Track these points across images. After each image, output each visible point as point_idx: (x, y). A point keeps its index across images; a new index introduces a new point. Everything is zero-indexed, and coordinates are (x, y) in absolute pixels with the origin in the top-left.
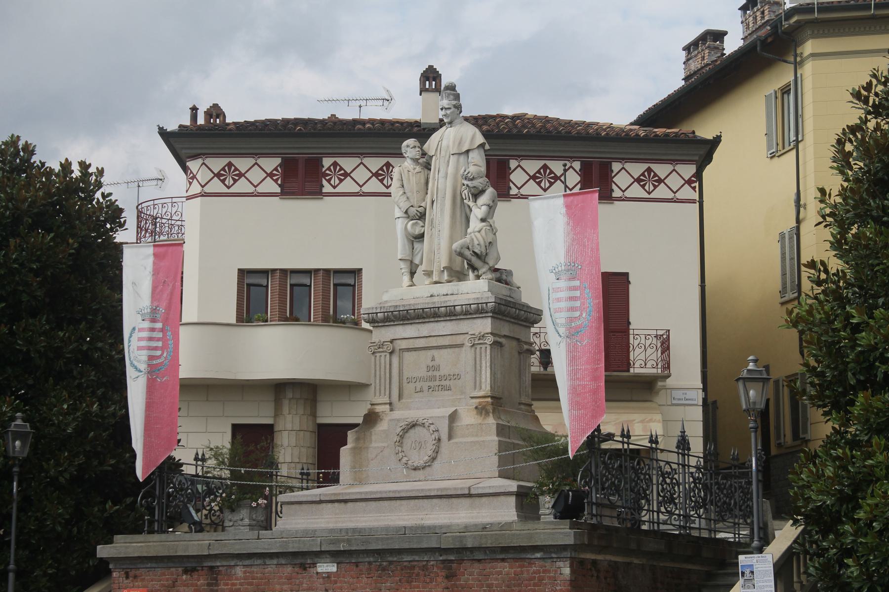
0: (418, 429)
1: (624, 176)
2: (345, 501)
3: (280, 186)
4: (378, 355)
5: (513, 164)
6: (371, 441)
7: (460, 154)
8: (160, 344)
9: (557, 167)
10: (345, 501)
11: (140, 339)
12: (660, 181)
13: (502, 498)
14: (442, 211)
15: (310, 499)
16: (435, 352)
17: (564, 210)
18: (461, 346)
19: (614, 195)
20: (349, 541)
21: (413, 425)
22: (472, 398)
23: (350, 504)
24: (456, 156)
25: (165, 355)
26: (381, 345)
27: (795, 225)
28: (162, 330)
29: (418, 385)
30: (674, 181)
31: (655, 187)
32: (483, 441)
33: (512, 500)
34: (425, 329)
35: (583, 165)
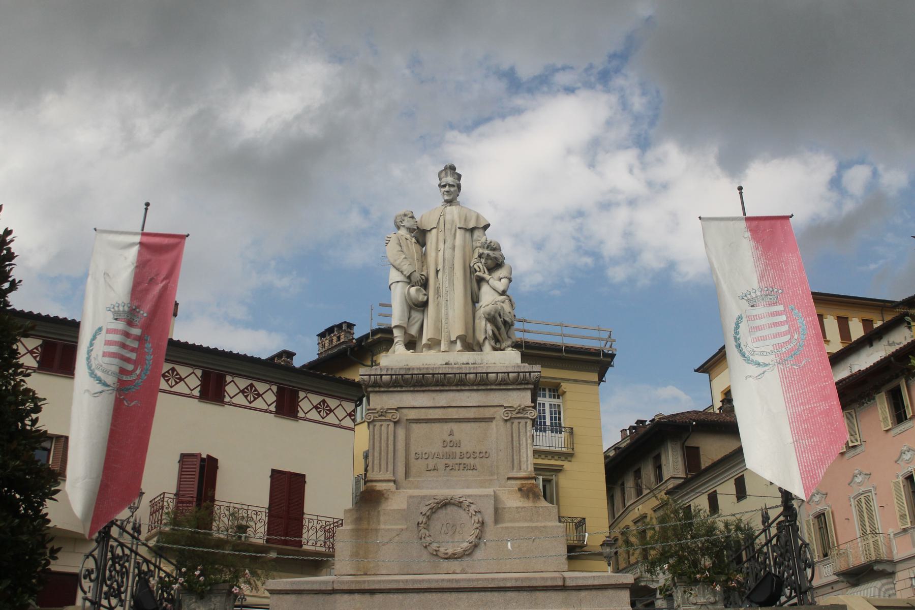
0: (450, 509)
1: (307, 403)
2: (372, 592)
3: (38, 362)
4: (378, 424)
5: (229, 378)
6: (379, 522)
7: (466, 230)
8: (133, 356)
9: (261, 387)
10: (372, 592)
11: (108, 343)
13: (610, 593)
14: (451, 282)
15: (316, 587)
16: (455, 426)
17: (748, 234)
18: (491, 420)
19: (299, 415)
21: (445, 504)
22: (509, 479)
23: (379, 597)
24: (463, 231)
25: (138, 372)
26: (383, 413)
27: (363, 472)
28: (140, 339)
29: (431, 463)
30: (340, 413)
31: (327, 414)
32: (544, 527)
33: (625, 595)
34: (443, 399)
35: (278, 388)
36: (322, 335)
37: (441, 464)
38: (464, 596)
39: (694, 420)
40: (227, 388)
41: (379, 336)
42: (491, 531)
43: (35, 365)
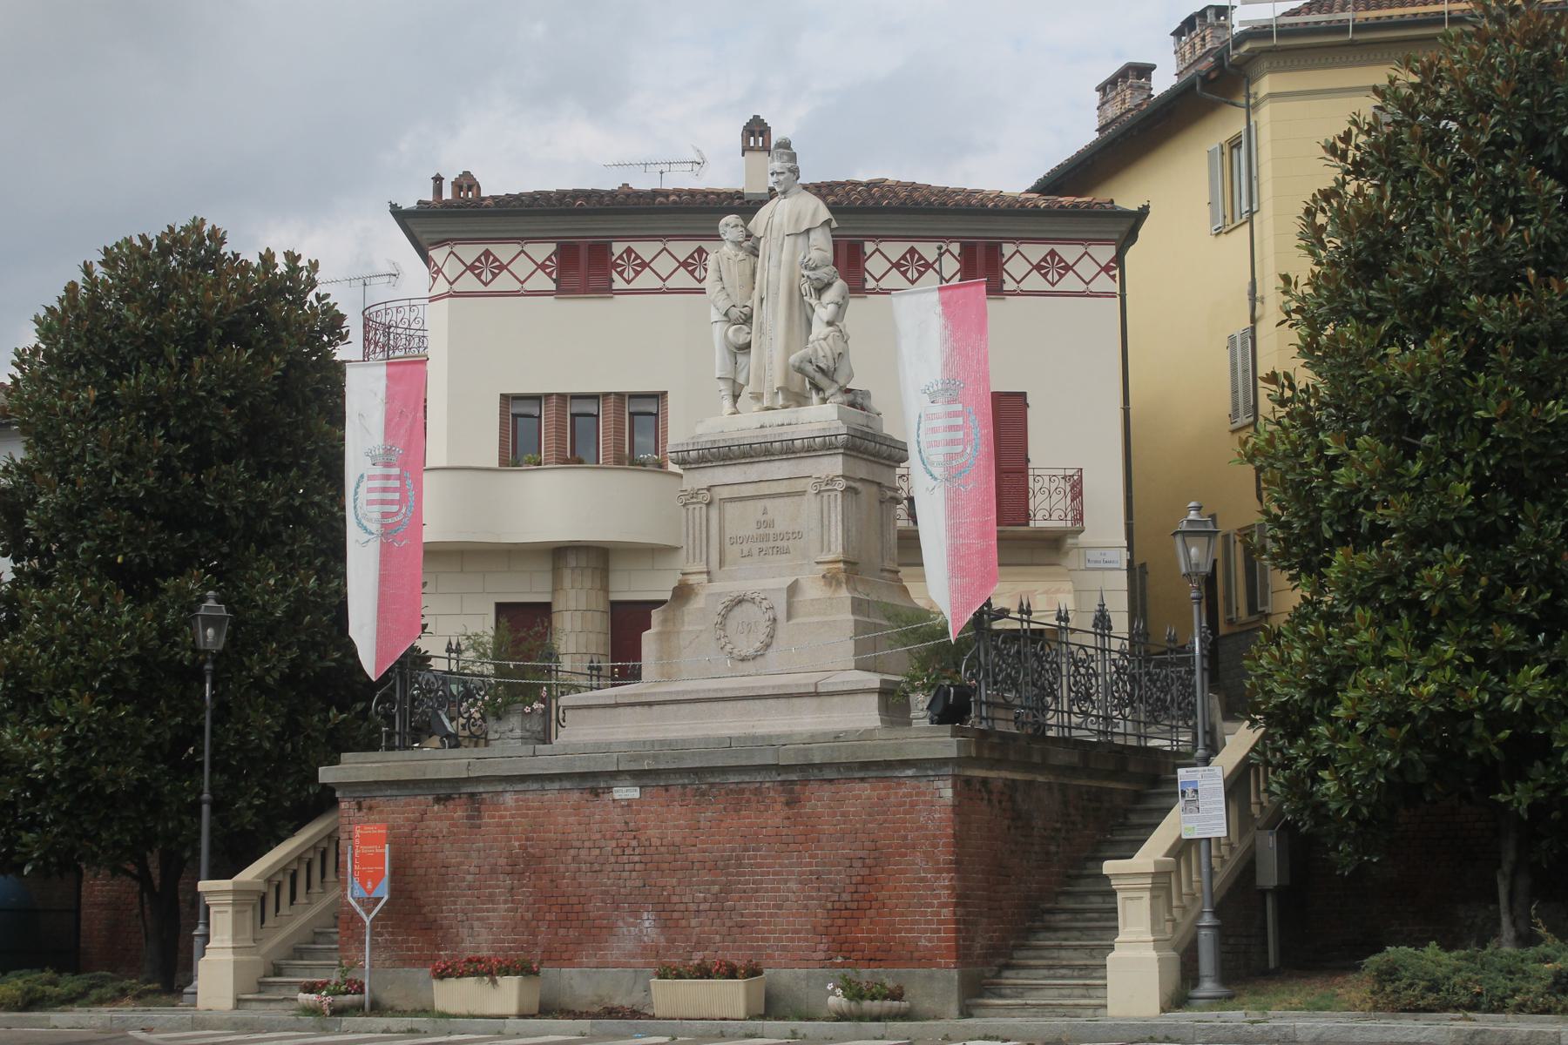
0: (745, 606)
1: (1018, 262)
2: (650, 704)
5: (869, 247)
9: (928, 251)
10: (650, 704)
11: (370, 490)
12: (1068, 268)
13: (860, 697)
16: (768, 503)
17: (939, 309)
20: (655, 757)
21: (740, 601)
23: (656, 708)
26: (695, 494)
27: (1249, 325)
30: (1087, 268)
33: (875, 698)
35: (964, 247)
36: (1178, 33)
37: (756, 547)
38: (729, 704)
39: (1411, 313)
40: (868, 265)
41: (1247, 47)
42: (783, 627)
43: (553, 287)
